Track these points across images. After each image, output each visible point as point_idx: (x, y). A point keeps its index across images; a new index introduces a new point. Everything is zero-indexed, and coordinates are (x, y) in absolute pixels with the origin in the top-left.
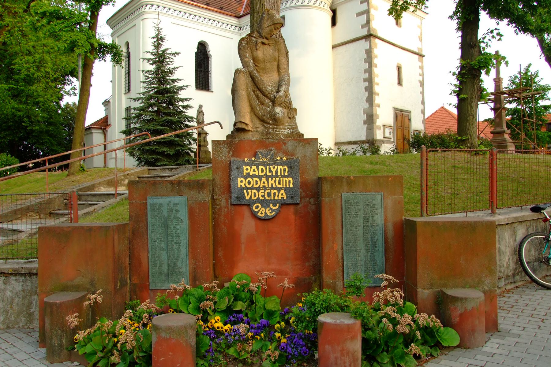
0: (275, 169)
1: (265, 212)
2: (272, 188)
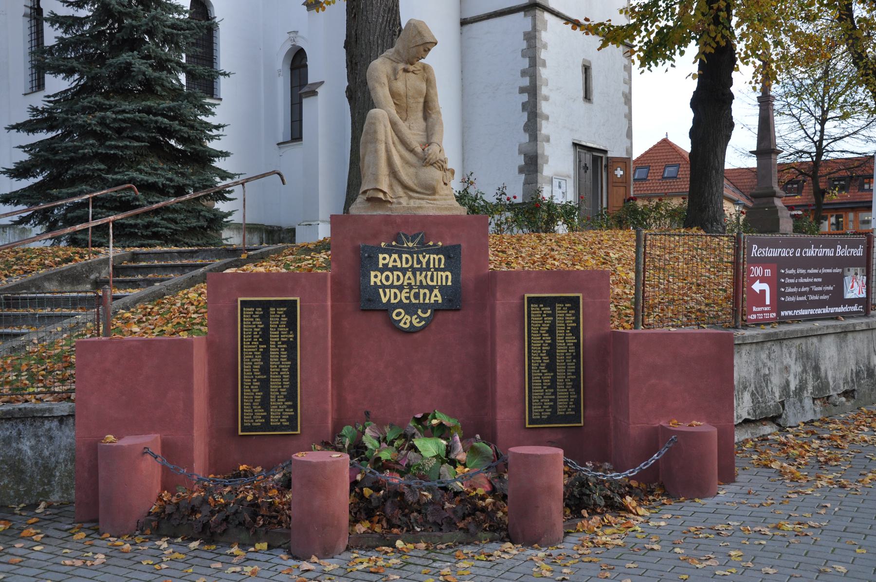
0: (426, 259)
2: (421, 286)
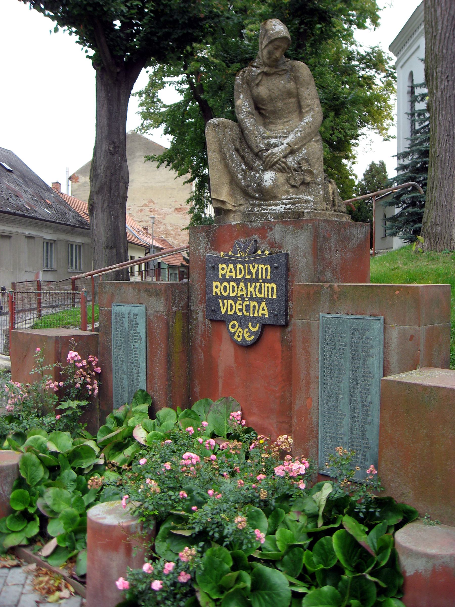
0: (256, 268)
1: (243, 335)
